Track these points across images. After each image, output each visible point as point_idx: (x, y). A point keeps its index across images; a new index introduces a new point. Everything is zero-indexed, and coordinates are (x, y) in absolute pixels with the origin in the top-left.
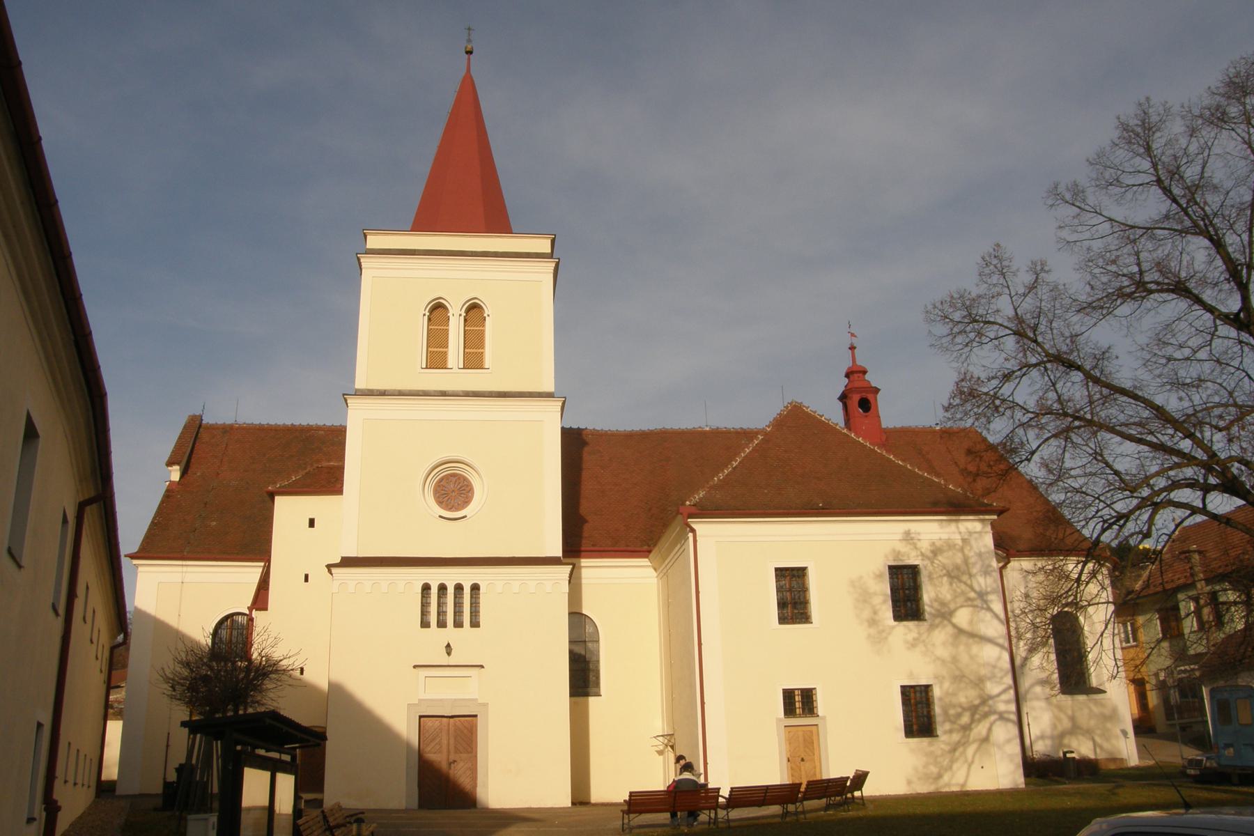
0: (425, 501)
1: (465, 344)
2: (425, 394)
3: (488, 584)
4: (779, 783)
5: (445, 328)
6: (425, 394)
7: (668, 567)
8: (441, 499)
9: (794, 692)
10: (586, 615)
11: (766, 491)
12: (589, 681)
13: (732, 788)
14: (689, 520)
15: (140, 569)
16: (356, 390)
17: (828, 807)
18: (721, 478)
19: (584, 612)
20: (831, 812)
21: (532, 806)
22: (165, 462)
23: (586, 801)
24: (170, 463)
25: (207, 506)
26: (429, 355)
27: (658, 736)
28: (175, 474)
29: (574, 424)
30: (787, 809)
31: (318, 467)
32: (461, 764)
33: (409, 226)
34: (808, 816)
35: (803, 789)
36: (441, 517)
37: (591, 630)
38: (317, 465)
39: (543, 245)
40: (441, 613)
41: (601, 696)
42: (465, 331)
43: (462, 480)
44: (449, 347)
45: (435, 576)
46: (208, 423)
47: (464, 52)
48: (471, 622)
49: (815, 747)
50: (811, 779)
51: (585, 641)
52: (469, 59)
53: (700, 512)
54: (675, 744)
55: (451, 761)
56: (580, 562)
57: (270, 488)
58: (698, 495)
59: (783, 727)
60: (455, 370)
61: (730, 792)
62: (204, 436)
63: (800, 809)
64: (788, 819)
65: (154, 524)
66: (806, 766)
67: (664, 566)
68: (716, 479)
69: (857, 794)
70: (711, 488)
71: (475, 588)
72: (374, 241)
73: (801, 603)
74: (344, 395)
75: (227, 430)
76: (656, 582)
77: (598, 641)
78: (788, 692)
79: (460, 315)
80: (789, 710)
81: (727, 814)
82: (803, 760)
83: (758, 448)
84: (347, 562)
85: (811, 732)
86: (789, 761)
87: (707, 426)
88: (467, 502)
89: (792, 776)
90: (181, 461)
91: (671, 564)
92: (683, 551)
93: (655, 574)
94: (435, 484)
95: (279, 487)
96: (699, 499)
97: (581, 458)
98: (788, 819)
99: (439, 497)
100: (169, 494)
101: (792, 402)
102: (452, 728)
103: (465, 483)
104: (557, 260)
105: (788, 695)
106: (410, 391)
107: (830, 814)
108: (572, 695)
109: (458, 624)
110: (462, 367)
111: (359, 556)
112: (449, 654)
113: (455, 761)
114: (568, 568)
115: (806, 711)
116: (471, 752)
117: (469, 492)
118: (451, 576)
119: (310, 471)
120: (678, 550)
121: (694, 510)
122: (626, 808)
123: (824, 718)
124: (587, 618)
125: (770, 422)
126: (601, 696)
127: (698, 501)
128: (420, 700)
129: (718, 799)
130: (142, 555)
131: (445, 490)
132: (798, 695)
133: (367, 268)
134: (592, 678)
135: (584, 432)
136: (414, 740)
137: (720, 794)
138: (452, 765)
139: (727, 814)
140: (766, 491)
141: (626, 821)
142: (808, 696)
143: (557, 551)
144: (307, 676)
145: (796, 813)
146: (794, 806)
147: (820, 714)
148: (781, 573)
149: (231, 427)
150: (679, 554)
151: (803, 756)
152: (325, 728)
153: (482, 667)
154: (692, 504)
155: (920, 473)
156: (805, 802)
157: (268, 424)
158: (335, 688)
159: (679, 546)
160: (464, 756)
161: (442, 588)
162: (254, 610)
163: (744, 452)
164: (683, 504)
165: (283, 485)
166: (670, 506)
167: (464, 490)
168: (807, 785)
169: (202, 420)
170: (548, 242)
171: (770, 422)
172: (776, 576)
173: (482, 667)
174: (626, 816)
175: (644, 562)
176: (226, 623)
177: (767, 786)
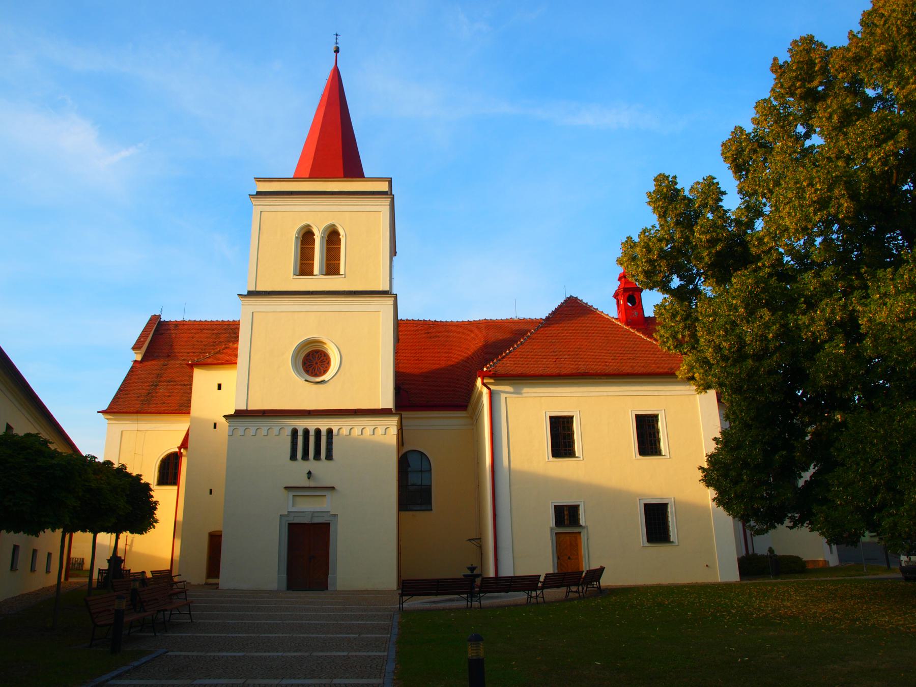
3: (234, 429)
35: (542, 579)
43: (323, 355)
45: (301, 424)
61: (545, 577)
82: (569, 558)
88: (325, 372)
109: (317, 456)
118: (312, 424)
143: (387, 400)
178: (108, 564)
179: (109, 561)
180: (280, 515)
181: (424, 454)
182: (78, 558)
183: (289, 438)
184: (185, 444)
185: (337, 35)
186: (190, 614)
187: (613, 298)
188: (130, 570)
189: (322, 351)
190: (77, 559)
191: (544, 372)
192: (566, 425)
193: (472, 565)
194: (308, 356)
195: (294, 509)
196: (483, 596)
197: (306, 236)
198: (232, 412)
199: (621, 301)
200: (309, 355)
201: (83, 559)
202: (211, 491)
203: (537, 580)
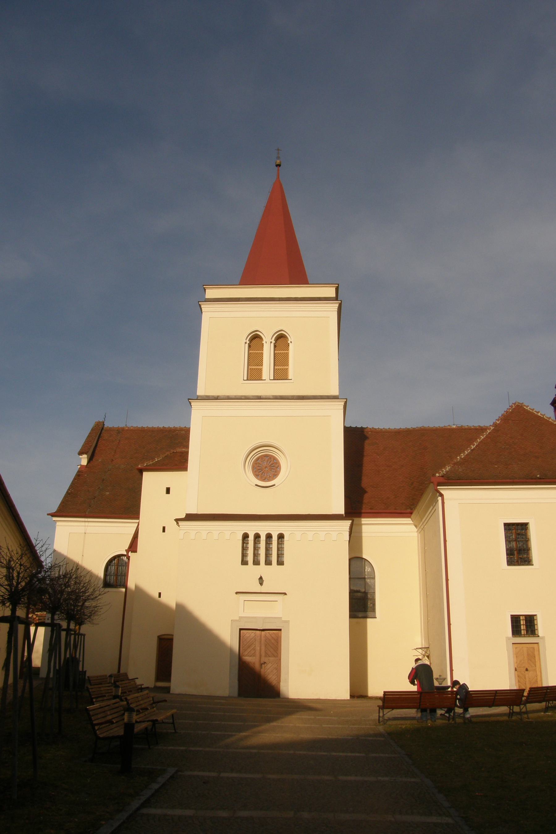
0: (246, 475)
1: (274, 363)
2: (246, 398)
3: (208, 533)
4: (508, 688)
5: (261, 352)
6: (246, 398)
7: (424, 524)
8: (257, 473)
9: (520, 618)
10: (365, 559)
11: (496, 466)
12: (367, 606)
14: (438, 487)
15: (58, 523)
16: (198, 396)
17: (547, 709)
18: (463, 457)
19: (364, 557)
20: (550, 714)
21: (321, 698)
22: (78, 452)
23: (364, 695)
24: (81, 453)
25: (104, 482)
26: (249, 371)
27: (417, 648)
28: (84, 460)
29: (356, 423)
30: (513, 710)
31: (174, 452)
32: (269, 665)
33: (238, 281)
34: (530, 715)
35: (525, 694)
36: (256, 485)
37: (369, 570)
38: (173, 451)
39: (330, 292)
40: (256, 555)
41: (376, 618)
42: (275, 354)
43: (272, 459)
45: (252, 528)
46: (108, 427)
47: (275, 165)
48: (278, 561)
49: (536, 660)
50: (534, 686)
51: (365, 578)
52: (278, 170)
53: (447, 481)
54: (430, 655)
55: (262, 662)
56: (361, 521)
57: (139, 466)
58: (445, 469)
59: (512, 644)
60: (268, 381)
62: (105, 435)
63: (524, 710)
64: (514, 718)
65: (68, 494)
66: (529, 675)
67: (421, 523)
68: (458, 457)
70: (455, 464)
71: (281, 537)
72: (211, 293)
73: (524, 550)
74: (189, 399)
75: (120, 431)
76: (417, 535)
77: (374, 578)
78: (515, 618)
79: (271, 342)
80: (516, 631)
82: (527, 670)
83: (489, 436)
84: (190, 517)
85: (534, 648)
86: (516, 670)
87: (454, 425)
88: (276, 475)
89: (519, 681)
90: (88, 452)
91: (426, 522)
92: (435, 510)
93: (416, 530)
94: (254, 462)
95: (146, 465)
96: (445, 472)
97: (363, 448)
98: (514, 718)
99: (256, 472)
100: (80, 474)
101: (515, 403)
102: (263, 639)
103: (275, 461)
104: (340, 302)
105: (515, 620)
106: (235, 396)
107: (549, 715)
108: (351, 616)
109: (268, 562)
110: (273, 379)
111: (198, 513)
112: (261, 584)
113: (265, 663)
114: (348, 523)
115: (530, 632)
116: (277, 656)
117: (277, 468)
118: (263, 528)
119: (168, 455)
120: (431, 511)
121: (442, 480)
122: (380, 703)
123: (543, 638)
124: (366, 561)
125: (499, 417)
126: (376, 618)
127: (445, 473)
128: (240, 617)
130: (58, 514)
131: (260, 467)
132: (523, 620)
133: (205, 312)
134: (370, 604)
135: (366, 430)
136: (236, 647)
138: (263, 665)
140: (496, 466)
141: (381, 714)
142: (530, 621)
143: (341, 510)
144: (164, 599)
145: (520, 713)
146: (518, 707)
147: (540, 635)
148: (508, 527)
149: (123, 429)
150: (431, 514)
151: (527, 667)
152: (173, 635)
153: (285, 594)
154: (441, 475)
156: (528, 705)
157: (147, 427)
158: (180, 607)
159: (432, 507)
160: (272, 659)
161: (257, 537)
162: (130, 552)
163: (480, 438)
164: (434, 475)
165: (148, 464)
166: (426, 481)
168: (529, 691)
169: (104, 425)
170: (334, 290)
171: (499, 417)
172: (505, 529)
173: (285, 594)
174: (381, 711)
175: (408, 520)
176: (114, 562)
177: (496, 691)
180: (232, 620)
181: (367, 560)
184: (133, 547)
185: (278, 150)
186: (173, 723)
188: (378, 706)
203: (521, 694)
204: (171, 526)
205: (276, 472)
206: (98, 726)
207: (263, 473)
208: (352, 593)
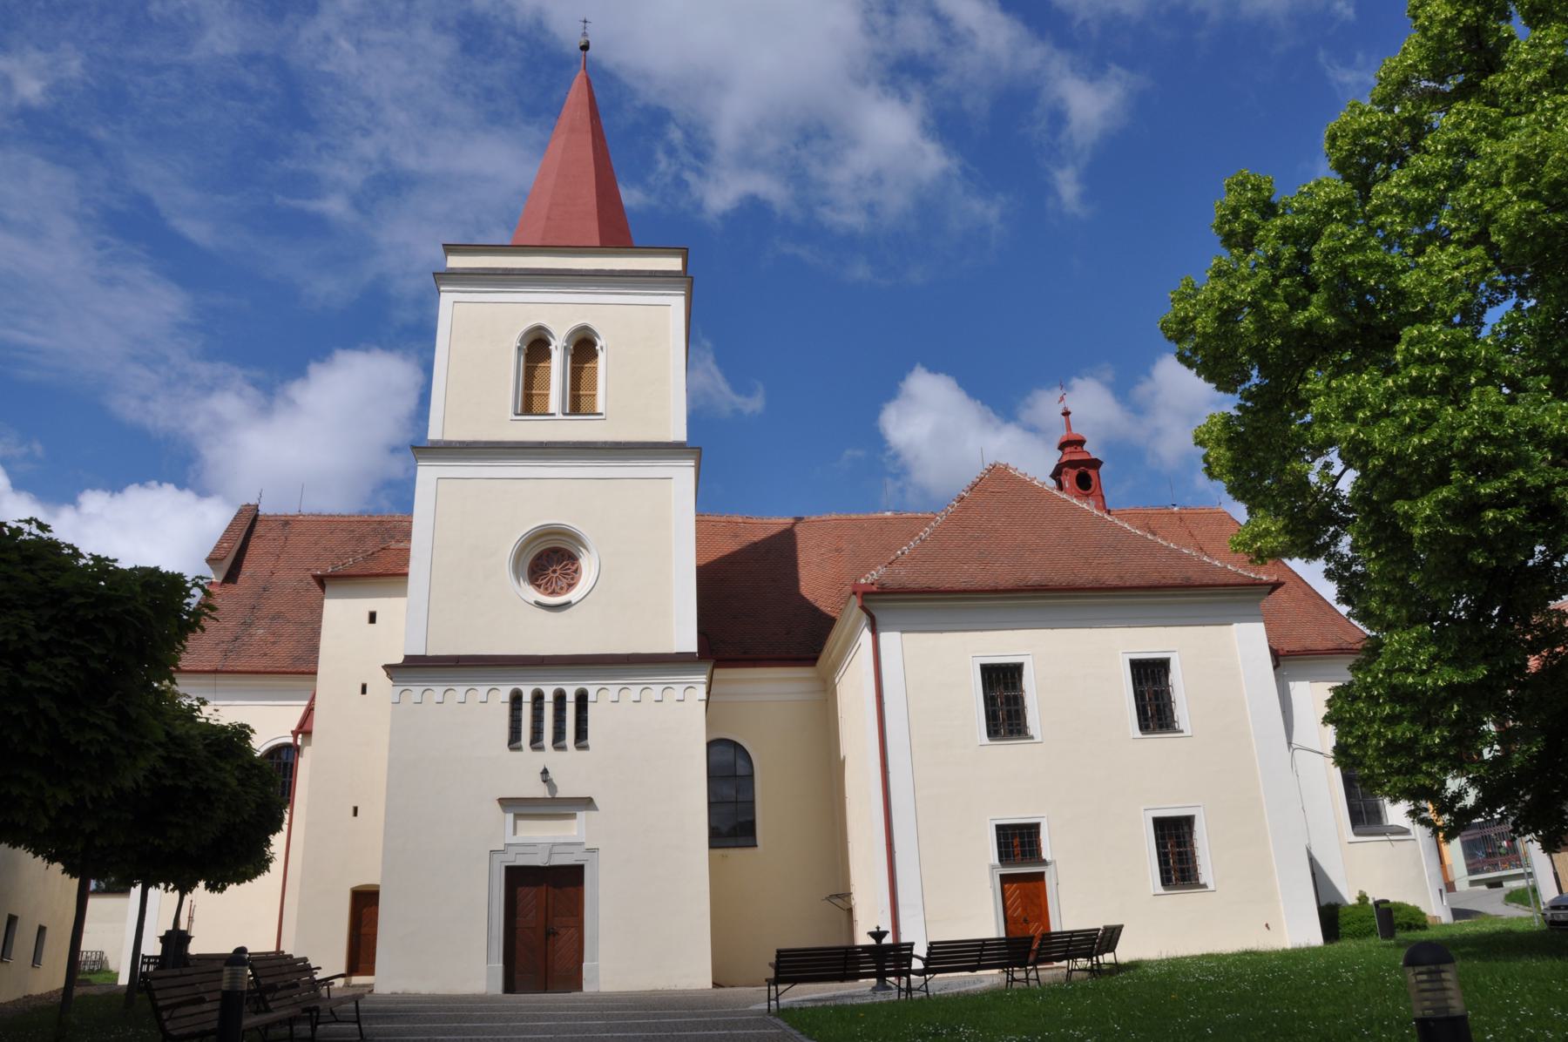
3: (402, 692)
13: (931, 943)
39: (674, 264)
44: (551, 389)
61: (929, 949)
69: (1108, 958)
71: (582, 699)
80: (1005, 855)
81: (926, 983)
88: (571, 586)
92: (860, 645)
129: (911, 961)
137: (914, 953)
139: (926, 983)
143: (686, 639)
155: (1165, 543)
167: (569, 569)
174: (773, 988)
177: (983, 940)
178: (161, 945)
179: (163, 939)
182: (92, 952)
183: (506, 708)
184: (304, 729)
185: (585, 22)
187: (1050, 479)
189: (566, 550)
190: (89, 954)
191: (969, 586)
192: (1010, 681)
193: (878, 928)
194: (538, 559)
195: (514, 840)
196: (930, 978)
197: (536, 346)
198: (399, 660)
199: (1067, 483)
200: (541, 556)
201: (102, 953)
202: (356, 809)
204: (381, 684)
205: (572, 579)
206: (169, 1012)
207: (549, 580)
208: (715, 745)
